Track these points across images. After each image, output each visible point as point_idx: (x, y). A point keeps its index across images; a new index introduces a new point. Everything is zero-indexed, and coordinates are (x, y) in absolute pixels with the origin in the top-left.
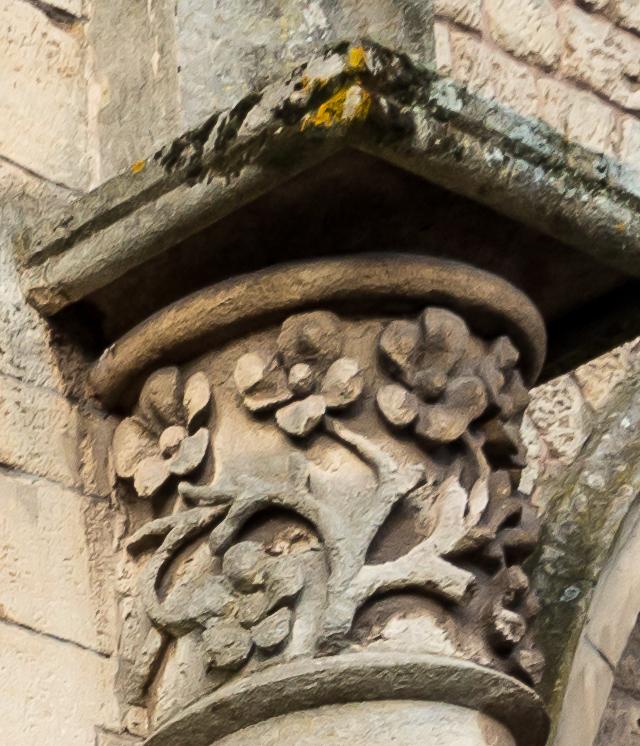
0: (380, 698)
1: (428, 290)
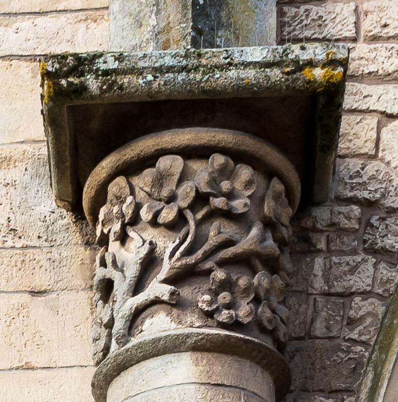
0: (138, 362)
1: (153, 150)
